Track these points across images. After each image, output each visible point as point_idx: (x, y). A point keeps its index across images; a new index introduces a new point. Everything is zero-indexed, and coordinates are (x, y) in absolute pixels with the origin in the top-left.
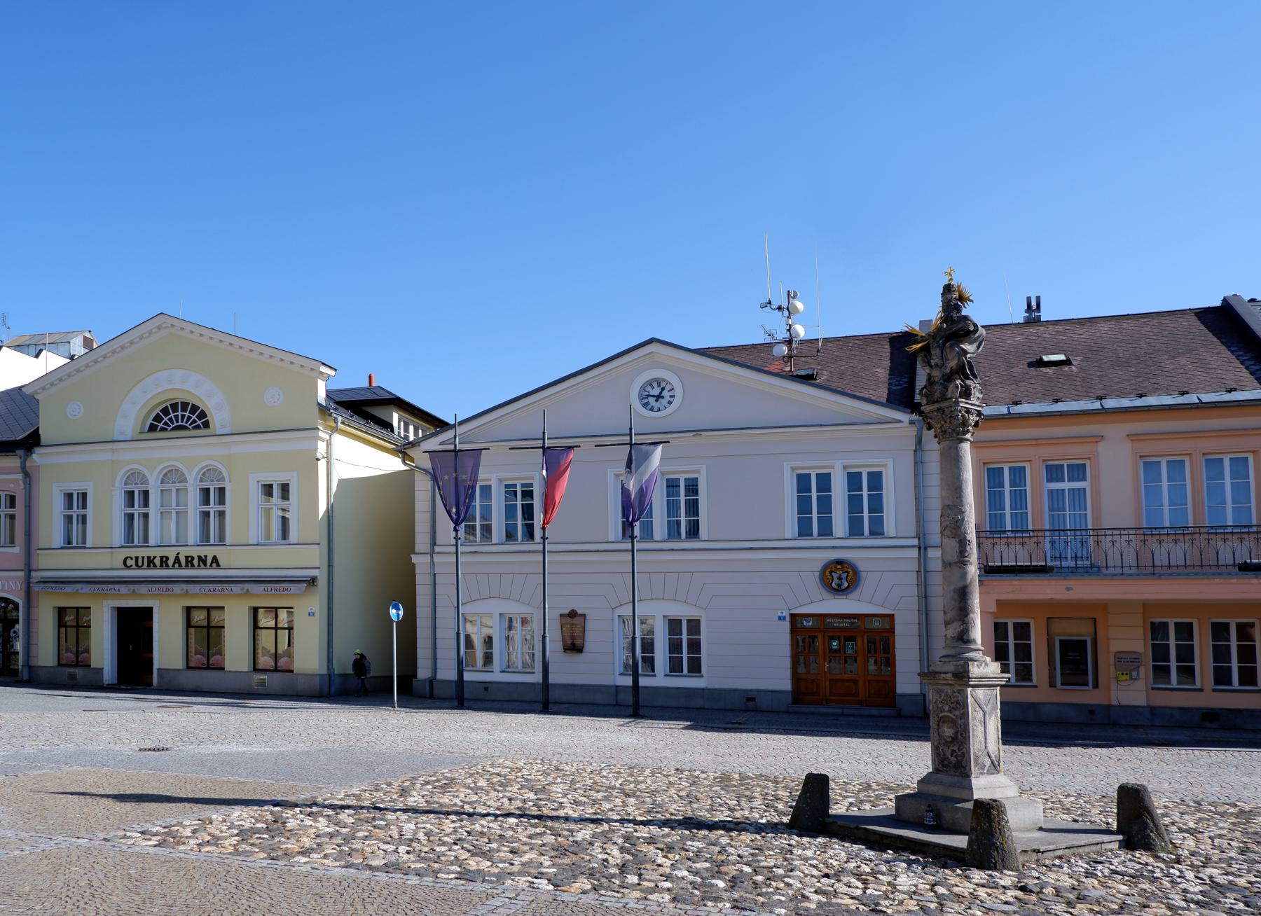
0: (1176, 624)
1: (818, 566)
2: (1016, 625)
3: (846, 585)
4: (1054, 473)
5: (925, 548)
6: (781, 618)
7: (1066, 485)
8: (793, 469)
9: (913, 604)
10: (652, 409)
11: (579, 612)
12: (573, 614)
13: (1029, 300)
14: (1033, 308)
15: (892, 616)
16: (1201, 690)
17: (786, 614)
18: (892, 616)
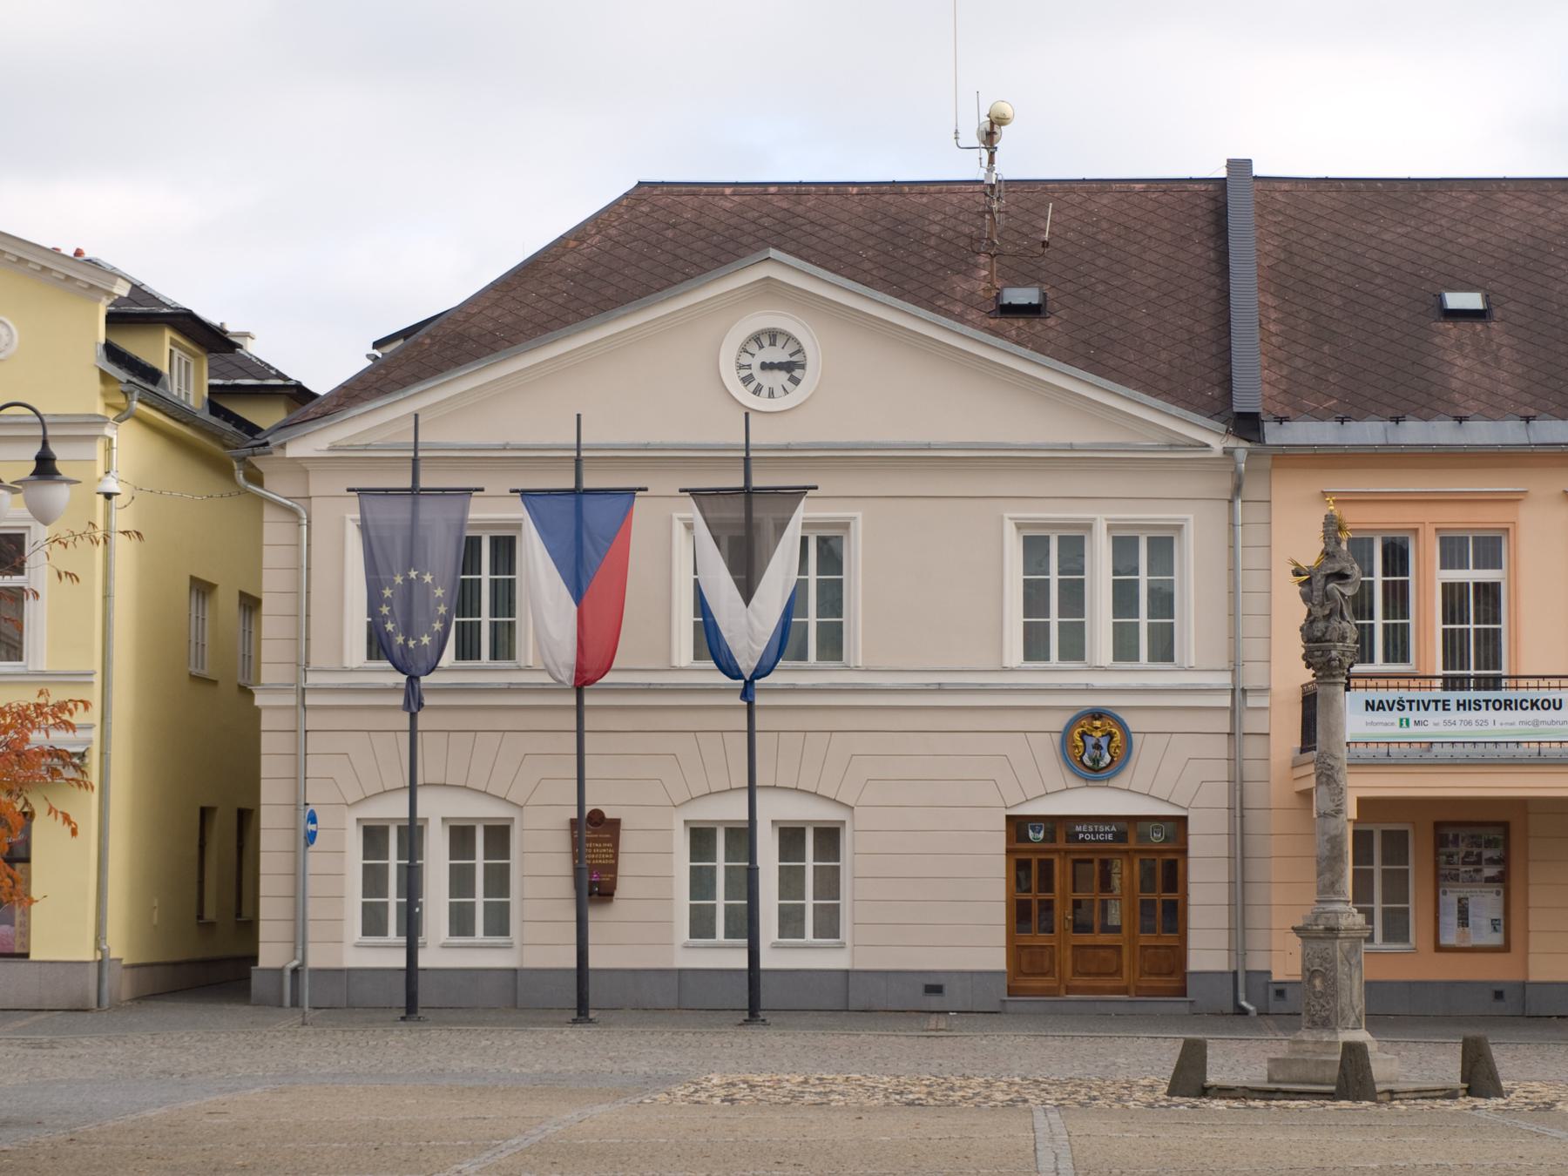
0: (1384, 832)
1: (1059, 722)
3: (1107, 758)
7: (1471, 575)
8: (1019, 527)
9: (1220, 796)
11: (609, 814)
14: (78, 253)
15: (1183, 820)
18: (1183, 820)
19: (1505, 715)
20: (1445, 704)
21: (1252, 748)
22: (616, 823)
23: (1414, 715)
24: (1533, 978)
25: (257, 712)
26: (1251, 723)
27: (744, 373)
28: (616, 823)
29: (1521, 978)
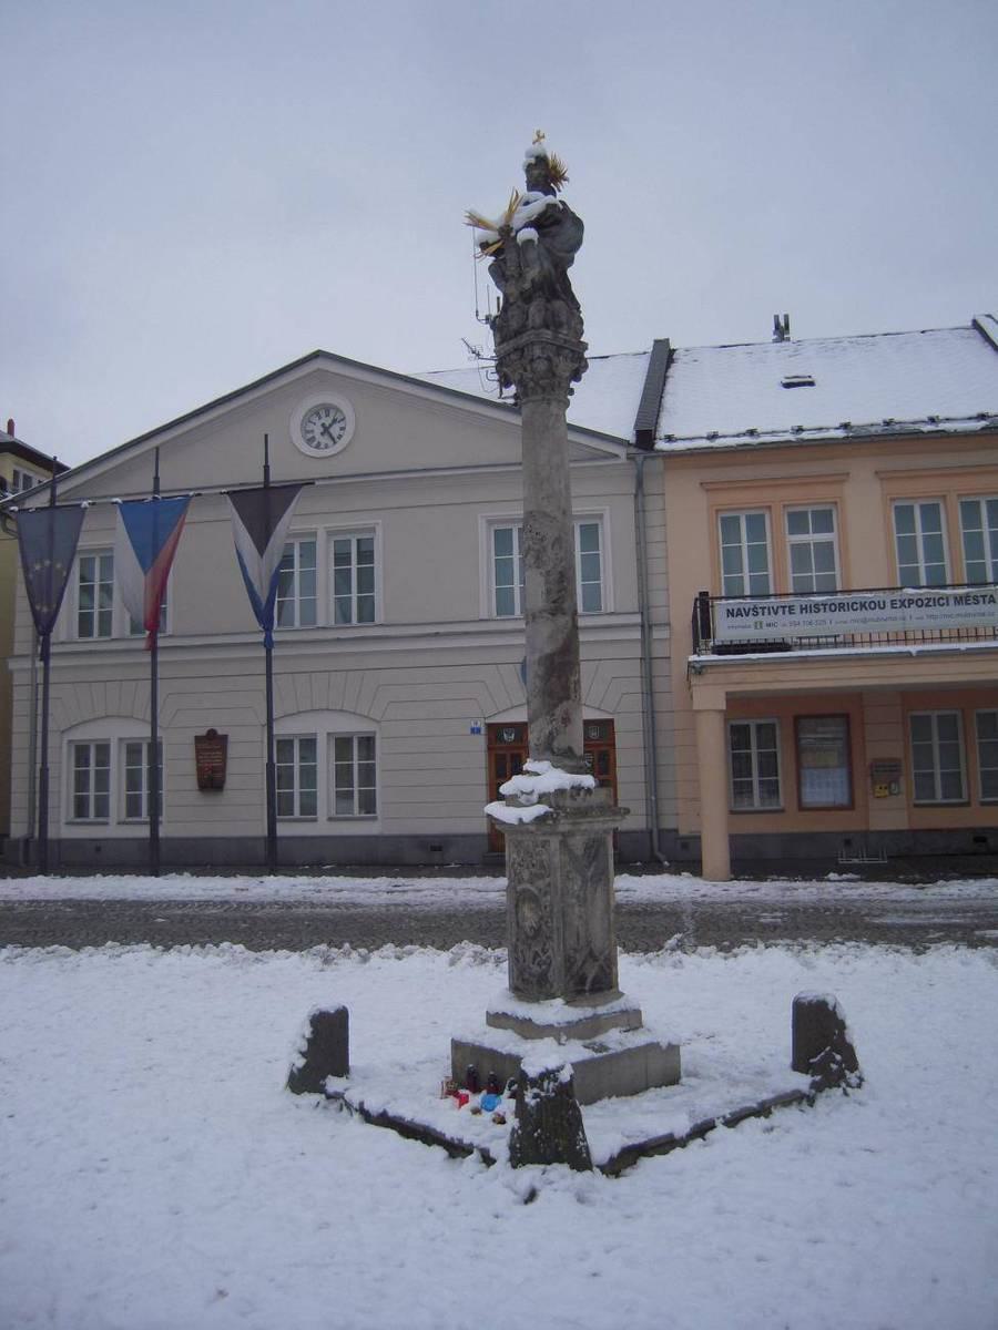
2: (759, 727)
4: (797, 522)
5: (650, 627)
6: (475, 731)
7: (812, 538)
8: (490, 522)
9: (635, 703)
10: (318, 447)
11: (220, 732)
12: (212, 734)
13: (777, 317)
15: (610, 722)
16: (782, 811)
17: (481, 724)
18: (610, 722)
19: (839, 615)
20: (791, 608)
21: (659, 668)
22: (225, 738)
23: (766, 619)
24: (872, 828)
25: (11, 673)
26: (658, 650)
27: (310, 436)
28: (225, 738)
29: (863, 828)
